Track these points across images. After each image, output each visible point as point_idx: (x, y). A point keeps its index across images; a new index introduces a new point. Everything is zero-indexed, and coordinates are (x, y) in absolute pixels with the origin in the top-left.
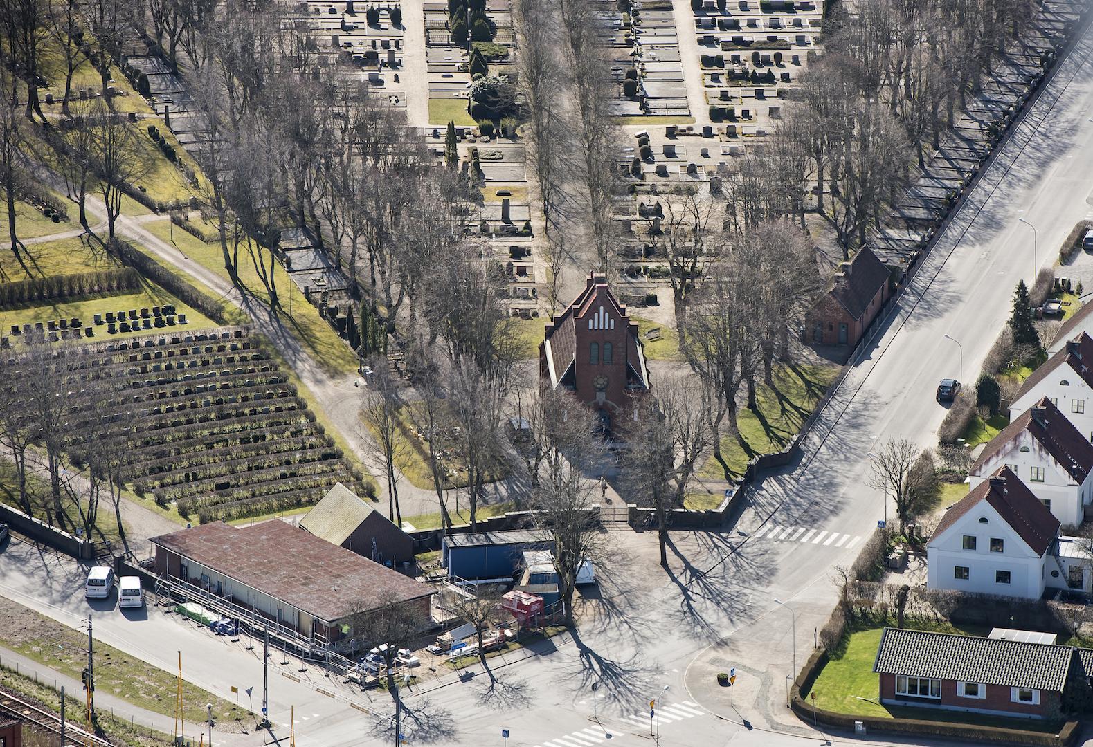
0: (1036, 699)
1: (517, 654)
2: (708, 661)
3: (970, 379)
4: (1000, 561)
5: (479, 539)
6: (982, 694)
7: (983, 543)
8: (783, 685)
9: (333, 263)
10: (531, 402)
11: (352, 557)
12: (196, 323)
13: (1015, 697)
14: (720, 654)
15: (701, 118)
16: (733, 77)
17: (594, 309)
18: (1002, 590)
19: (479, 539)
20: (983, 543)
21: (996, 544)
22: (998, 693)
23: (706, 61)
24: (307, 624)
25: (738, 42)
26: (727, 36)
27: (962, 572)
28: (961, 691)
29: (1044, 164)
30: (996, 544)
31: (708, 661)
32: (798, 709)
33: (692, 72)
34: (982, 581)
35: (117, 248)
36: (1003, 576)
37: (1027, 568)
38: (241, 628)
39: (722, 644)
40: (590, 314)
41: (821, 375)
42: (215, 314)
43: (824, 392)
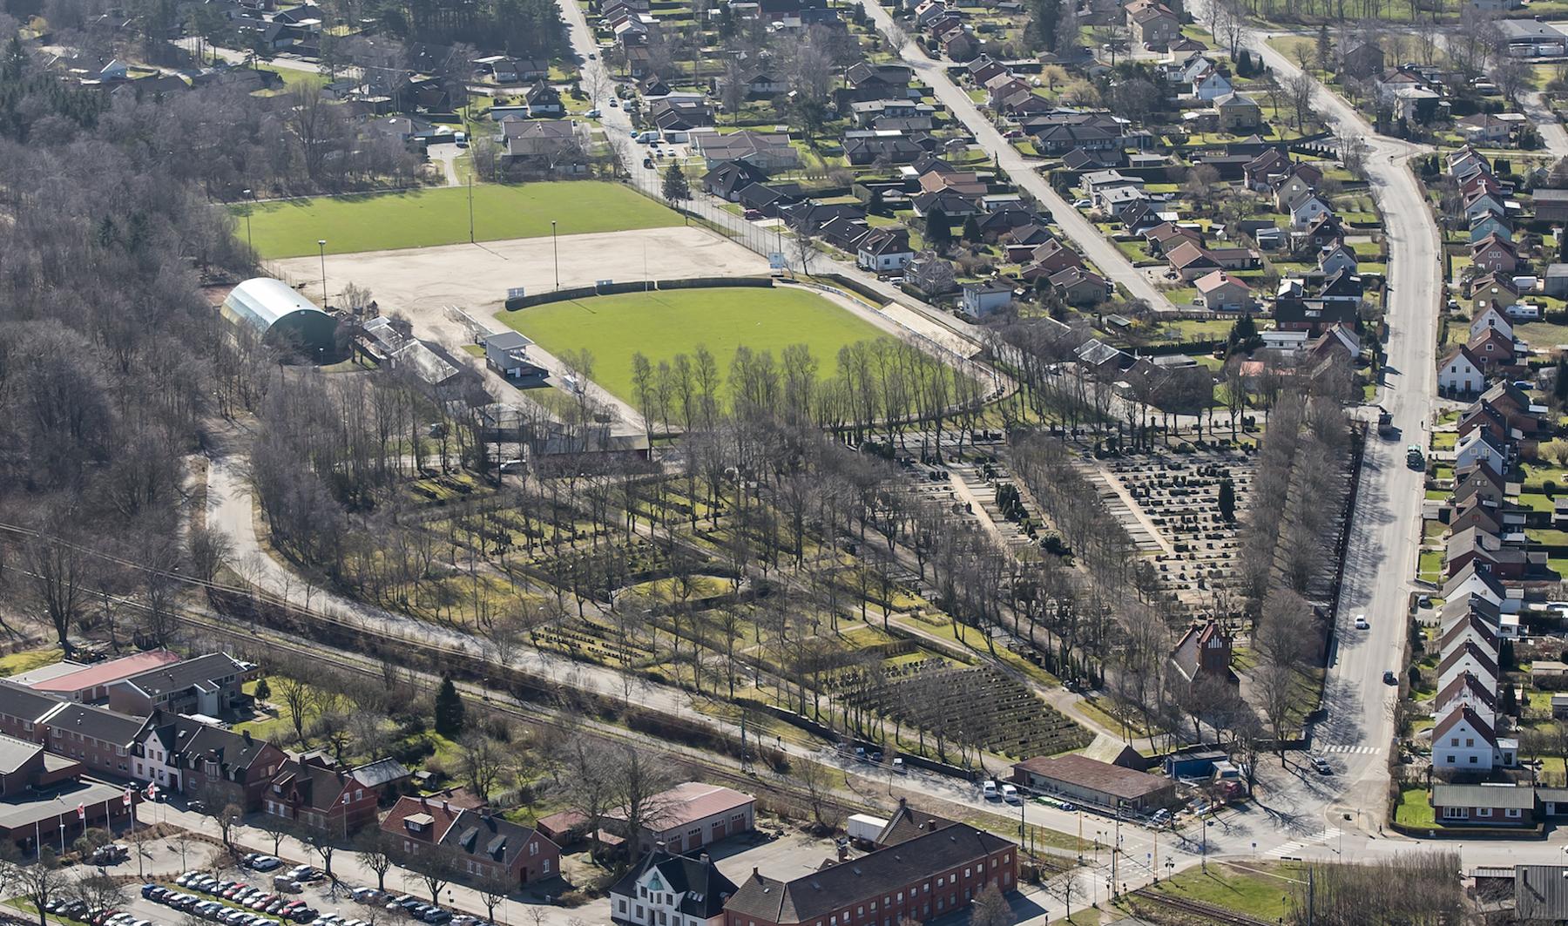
0: (1519, 815)
1: (1231, 812)
2: (1339, 811)
3: (1396, 669)
4: (1471, 751)
5: (1187, 757)
6: (1490, 814)
7: (1463, 743)
8: (1380, 817)
9: (1016, 633)
10: (560, 817)
11: (1119, 769)
12: (959, 666)
13: (1508, 814)
14: (1338, 806)
15: (1173, 554)
16: (1175, 529)
17: (1211, 637)
18: (1473, 765)
19: (1187, 757)
20: (1463, 743)
21: (1470, 743)
22: (1499, 812)
23: (1156, 522)
24: (1114, 800)
25: (1167, 511)
26: (1159, 509)
27: (1451, 759)
28: (1479, 813)
29: (1374, 565)
30: (1470, 743)
31: (1339, 811)
32: (1394, 827)
33: (1153, 531)
34: (1462, 761)
35: (890, 631)
36: (1473, 760)
37: (1484, 753)
38: (1076, 808)
39: (1336, 801)
40: (1209, 640)
41: (656, 801)
42: (966, 660)
43: (1323, 681)
